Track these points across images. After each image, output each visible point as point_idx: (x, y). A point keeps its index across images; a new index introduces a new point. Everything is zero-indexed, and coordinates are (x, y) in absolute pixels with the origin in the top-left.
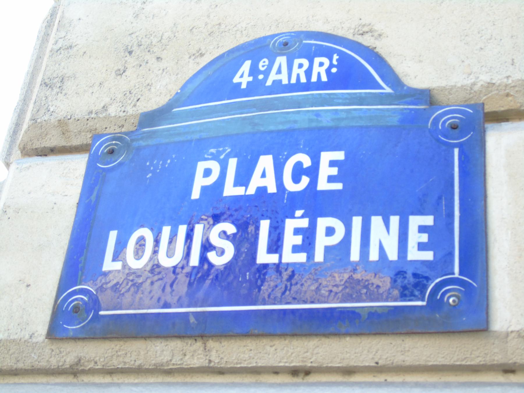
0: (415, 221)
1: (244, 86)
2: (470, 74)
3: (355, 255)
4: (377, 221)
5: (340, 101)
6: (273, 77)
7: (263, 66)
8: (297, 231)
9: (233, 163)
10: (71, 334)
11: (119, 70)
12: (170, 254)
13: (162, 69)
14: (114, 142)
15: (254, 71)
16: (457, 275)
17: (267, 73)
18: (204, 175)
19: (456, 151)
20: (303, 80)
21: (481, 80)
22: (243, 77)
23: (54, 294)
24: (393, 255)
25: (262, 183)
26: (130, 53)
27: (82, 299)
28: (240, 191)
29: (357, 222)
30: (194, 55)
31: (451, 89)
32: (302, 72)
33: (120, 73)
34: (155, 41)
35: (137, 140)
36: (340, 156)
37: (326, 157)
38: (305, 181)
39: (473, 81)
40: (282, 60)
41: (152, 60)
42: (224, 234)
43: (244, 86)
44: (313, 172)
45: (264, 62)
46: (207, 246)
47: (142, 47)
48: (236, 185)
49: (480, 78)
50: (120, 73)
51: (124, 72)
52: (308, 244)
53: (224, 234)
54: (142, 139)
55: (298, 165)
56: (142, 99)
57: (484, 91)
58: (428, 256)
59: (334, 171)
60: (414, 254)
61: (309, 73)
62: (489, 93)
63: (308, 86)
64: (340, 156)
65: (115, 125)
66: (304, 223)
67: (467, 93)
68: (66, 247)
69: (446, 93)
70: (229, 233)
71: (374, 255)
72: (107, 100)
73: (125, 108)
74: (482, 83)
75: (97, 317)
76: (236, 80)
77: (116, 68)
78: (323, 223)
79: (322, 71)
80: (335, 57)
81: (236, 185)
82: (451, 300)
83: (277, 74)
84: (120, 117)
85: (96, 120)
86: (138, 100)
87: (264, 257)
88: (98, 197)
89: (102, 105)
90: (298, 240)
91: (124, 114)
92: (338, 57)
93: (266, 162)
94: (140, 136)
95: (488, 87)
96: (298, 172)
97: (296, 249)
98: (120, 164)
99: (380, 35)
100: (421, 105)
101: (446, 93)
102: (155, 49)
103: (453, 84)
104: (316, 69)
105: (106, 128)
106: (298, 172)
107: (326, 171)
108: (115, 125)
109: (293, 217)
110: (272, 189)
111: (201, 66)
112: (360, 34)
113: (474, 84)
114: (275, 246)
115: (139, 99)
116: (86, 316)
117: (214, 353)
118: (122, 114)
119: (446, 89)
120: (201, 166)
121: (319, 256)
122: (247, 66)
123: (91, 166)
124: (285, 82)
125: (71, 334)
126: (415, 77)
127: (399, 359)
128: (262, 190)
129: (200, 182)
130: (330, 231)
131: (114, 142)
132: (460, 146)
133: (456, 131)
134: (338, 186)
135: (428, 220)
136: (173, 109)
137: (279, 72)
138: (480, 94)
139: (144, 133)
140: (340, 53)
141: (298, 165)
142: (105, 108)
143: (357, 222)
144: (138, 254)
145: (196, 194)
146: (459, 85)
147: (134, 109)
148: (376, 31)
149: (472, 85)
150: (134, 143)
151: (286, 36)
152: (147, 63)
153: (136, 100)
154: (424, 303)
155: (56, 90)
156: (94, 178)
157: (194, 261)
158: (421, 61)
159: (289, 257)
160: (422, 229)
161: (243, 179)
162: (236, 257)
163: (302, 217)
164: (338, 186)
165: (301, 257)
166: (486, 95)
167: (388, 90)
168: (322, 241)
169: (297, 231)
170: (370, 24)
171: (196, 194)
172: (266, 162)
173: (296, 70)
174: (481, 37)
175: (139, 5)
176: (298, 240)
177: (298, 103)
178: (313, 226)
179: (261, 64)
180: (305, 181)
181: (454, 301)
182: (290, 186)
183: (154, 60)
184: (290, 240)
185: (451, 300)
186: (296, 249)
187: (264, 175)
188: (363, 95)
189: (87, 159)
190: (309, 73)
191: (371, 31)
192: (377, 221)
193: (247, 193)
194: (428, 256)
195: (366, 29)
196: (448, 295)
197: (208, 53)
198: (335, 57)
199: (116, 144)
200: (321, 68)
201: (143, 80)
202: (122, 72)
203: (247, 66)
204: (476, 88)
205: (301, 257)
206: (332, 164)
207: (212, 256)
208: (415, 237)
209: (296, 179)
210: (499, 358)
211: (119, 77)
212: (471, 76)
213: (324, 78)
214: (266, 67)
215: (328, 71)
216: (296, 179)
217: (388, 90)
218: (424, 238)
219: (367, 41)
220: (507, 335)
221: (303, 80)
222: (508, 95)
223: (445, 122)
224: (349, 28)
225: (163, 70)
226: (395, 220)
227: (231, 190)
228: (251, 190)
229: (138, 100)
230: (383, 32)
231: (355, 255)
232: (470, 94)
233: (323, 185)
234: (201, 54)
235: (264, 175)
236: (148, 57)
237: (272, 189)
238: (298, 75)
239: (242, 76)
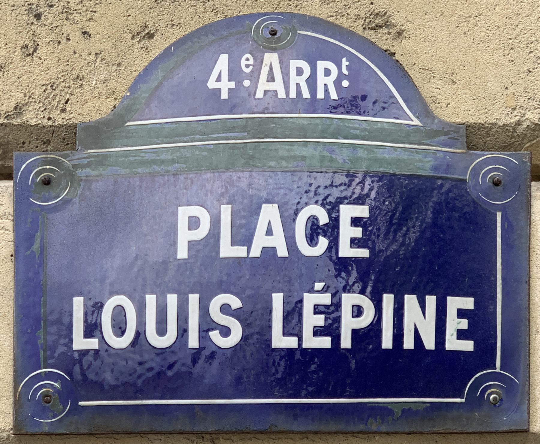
0: (455, 303)
1: (224, 95)
2: (514, 109)
3: (387, 342)
4: (410, 301)
5: (358, 132)
6: (263, 85)
7: (247, 66)
9: (226, 212)
10: (46, 429)
11: (27, 46)
12: (162, 331)
13: (93, 53)
14: (48, 167)
15: (235, 73)
16: (498, 370)
17: (255, 76)
19: (499, 215)
20: (306, 94)
21: (527, 119)
24: (430, 344)
25: (269, 242)
26: (38, 16)
27: (52, 385)
28: (240, 252)
29: (388, 300)
30: (138, 34)
31: (491, 129)
35: (83, 167)
37: (347, 212)
38: (323, 242)
39: (517, 118)
42: (225, 309)
43: (224, 95)
44: (332, 230)
45: (248, 59)
46: (207, 325)
47: (54, 9)
48: (233, 244)
49: (527, 116)
51: (35, 51)
53: (225, 309)
54: (89, 165)
55: (313, 221)
56: (73, 99)
57: (529, 135)
58: (468, 346)
60: (452, 343)
61: (312, 82)
62: (535, 139)
63: (313, 104)
65: (37, 139)
66: (326, 299)
67: (508, 136)
68: (11, 316)
69: (484, 133)
70: (234, 307)
71: (408, 343)
72: (18, 97)
73: (49, 113)
74: (528, 123)
77: (20, 43)
79: (330, 81)
80: (345, 63)
81: (233, 244)
82: (492, 397)
83: (268, 81)
84: (44, 127)
85: (8, 129)
86: (66, 103)
87: (281, 341)
88: (42, 249)
89: (13, 105)
90: (320, 320)
91: (50, 123)
92: (347, 63)
93: (270, 214)
94: (85, 162)
95: (534, 130)
96: (314, 231)
97: (318, 332)
99: (399, 34)
100: (457, 148)
101: (484, 133)
102: (77, 17)
103: (494, 121)
105: (24, 143)
107: (348, 232)
108: (37, 139)
109: (311, 290)
110: (282, 252)
112: (372, 29)
113: (519, 123)
115: (68, 100)
116: (61, 407)
118: (45, 122)
119: (484, 128)
120: (184, 213)
121: (346, 343)
125: (47, 428)
126: (447, 106)
128: (269, 252)
129: (185, 237)
131: (48, 167)
132: (503, 209)
133: (500, 188)
134: (364, 253)
135: (468, 303)
136: (126, 123)
137: (271, 78)
138: (523, 140)
139: (90, 156)
140: (351, 57)
141: (313, 221)
142: (18, 109)
143: (388, 300)
145: (182, 253)
146: (501, 123)
147: (63, 115)
148: (394, 25)
149: (516, 124)
150: (79, 171)
151: (272, 19)
152: (68, 40)
153: (63, 101)
154: (463, 400)
156: (29, 220)
157: (193, 342)
158: (454, 82)
159: (311, 342)
160: (461, 313)
162: (245, 338)
163: (324, 290)
164: (364, 253)
165: (325, 342)
166: (529, 141)
167: (416, 122)
170: (385, 13)
171: (182, 253)
172: (270, 214)
174: (530, 52)
176: (320, 320)
177: (303, 131)
179: (243, 62)
180: (323, 242)
181: (495, 398)
183: (78, 34)
184: (311, 320)
185: (492, 397)
186: (318, 332)
187: (269, 232)
188: (386, 126)
189: (11, 190)
190: (312, 82)
192: (410, 301)
193: (251, 255)
194: (468, 346)
195: (379, 21)
196: (489, 391)
197: (159, 33)
198: (345, 63)
199: (51, 170)
200: (329, 78)
201: (69, 68)
202: (32, 50)
204: (520, 129)
207: (215, 336)
208: (454, 324)
209: (312, 240)
211: (28, 59)
212: (515, 113)
213: (334, 95)
214: (251, 67)
215: (337, 83)
216: (312, 240)
217: (416, 122)
218: (464, 324)
219: (382, 40)
224: (358, 17)
225: (97, 54)
226: (431, 301)
227: (228, 250)
228: (255, 252)
229: (66, 103)
230: (403, 28)
231: (387, 342)
232: (511, 138)
233: (346, 250)
234: (148, 33)
235: (269, 232)
236: (67, 29)
237: (282, 252)
238: (298, 85)
239: (219, 79)
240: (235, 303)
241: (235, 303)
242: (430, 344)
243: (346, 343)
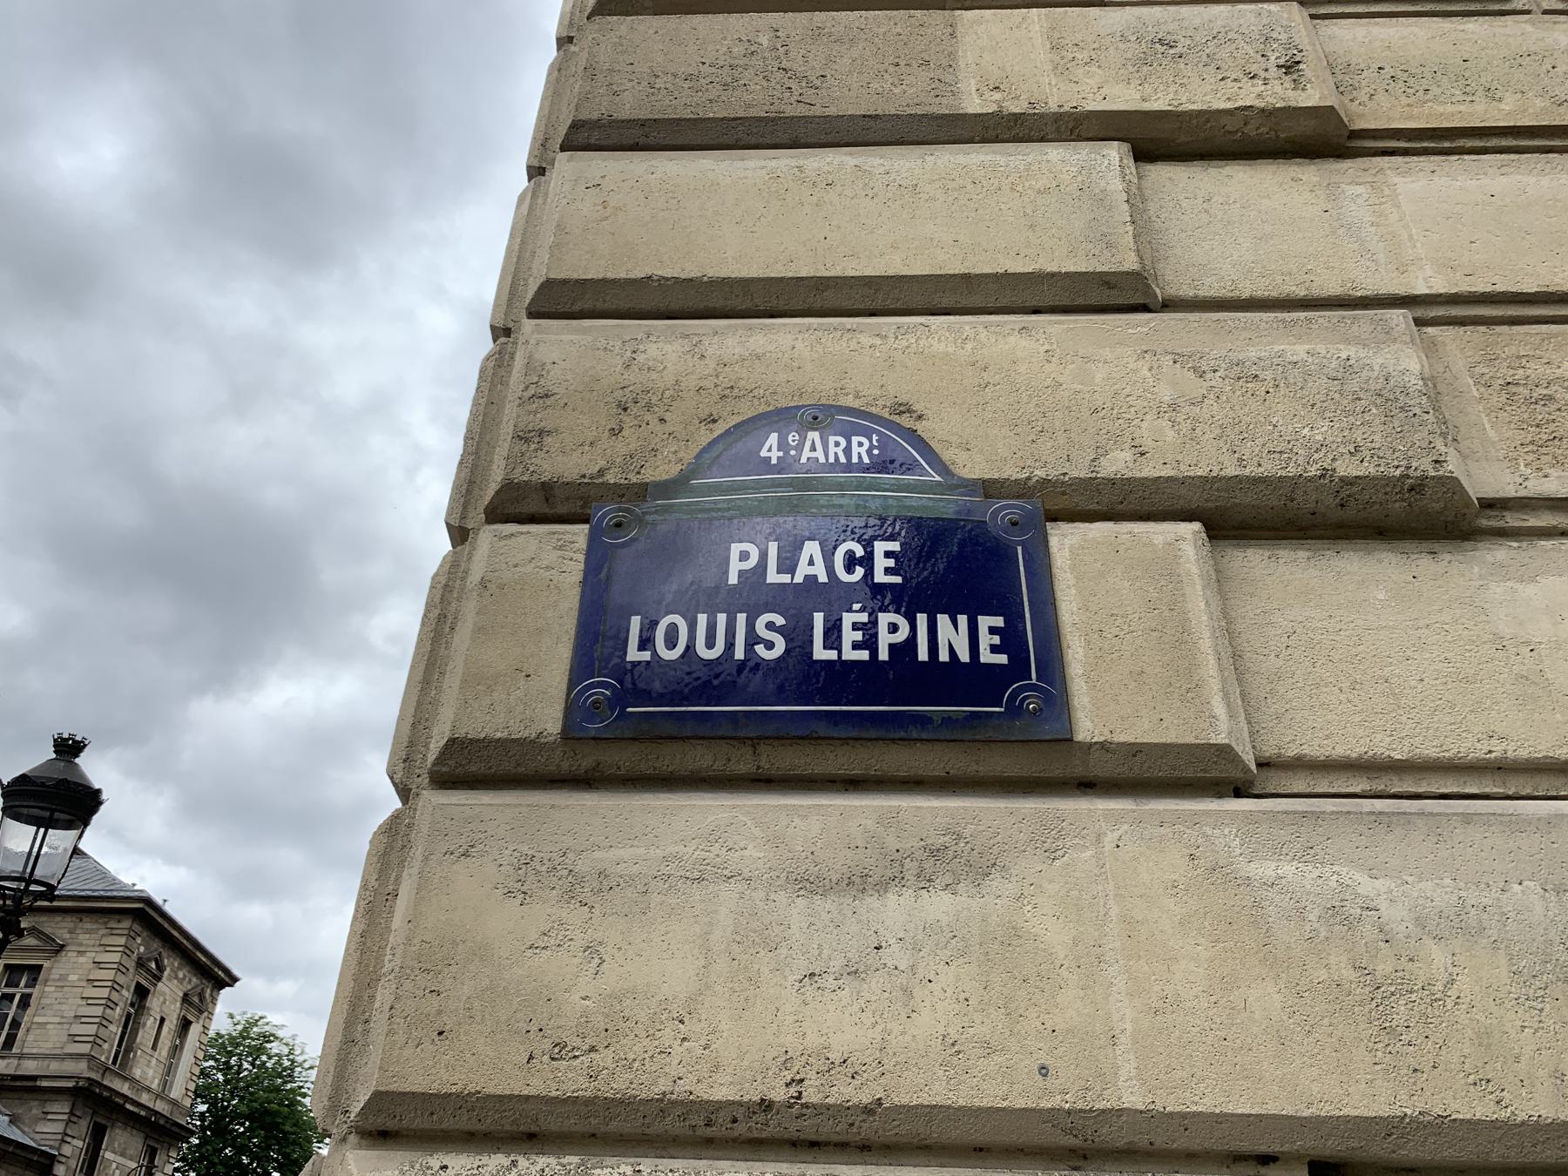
0: (985, 622)
1: (774, 461)
3: (923, 655)
4: (943, 620)
6: (806, 454)
8: (856, 627)
9: (773, 548)
10: (593, 734)
12: (710, 644)
15: (783, 445)
17: (800, 448)
18: (740, 558)
19: (1019, 549)
20: (843, 460)
22: (770, 448)
23: (564, 686)
24: (964, 657)
26: (625, 409)
28: (786, 578)
32: (840, 450)
33: (615, 433)
34: (654, 399)
36: (895, 546)
38: (860, 572)
40: (814, 436)
41: (654, 421)
42: (770, 626)
43: (774, 461)
44: (868, 561)
46: (752, 639)
50: (615, 433)
52: (870, 643)
53: (770, 626)
55: (850, 556)
59: (891, 563)
61: (848, 451)
63: (849, 467)
64: (895, 546)
66: (864, 618)
72: (602, 463)
75: (623, 714)
76: (764, 453)
78: (884, 619)
87: (820, 653)
93: (812, 548)
96: (851, 562)
98: (633, 540)
104: (855, 449)
106: (851, 562)
107: (881, 563)
109: (850, 610)
110: (823, 578)
111: (716, 434)
113: (1029, 478)
114: (646, 643)
117: (764, 758)
120: (736, 548)
121: (883, 655)
122: (773, 438)
123: (593, 539)
124: (822, 460)
127: (645, 768)
129: (735, 567)
130: (894, 628)
132: (1023, 543)
134: (898, 580)
135: (999, 622)
137: (813, 449)
140: (879, 433)
141: (850, 556)
142: (601, 472)
143: (922, 619)
144: (671, 643)
145: (733, 579)
155: (533, 447)
157: (739, 654)
159: (850, 654)
160: (992, 631)
161: (788, 566)
162: (787, 651)
163: (862, 610)
164: (898, 580)
165: (864, 655)
168: (885, 640)
169: (856, 627)
171: (733, 579)
172: (812, 548)
173: (832, 449)
175: (629, 354)
177: (841, 486)
178: (874, 623)
179: (790, 438)
180: (860, 572)
182: (844, 577)
184: (849, 636)
187: (811, 563)
190: (848, 451)
191: (909, 411)
192: (943, 620)
194: (1002, 659)
198: (875, 437)
200: (861, 449)
203: (773, 438)
204: (1030, 483)
205: (864, 655)
206: (888, 554)
207: (760, 649)
208: (985, 640)
209: (849, 568)
210: (1079, 771)
213: (866, 460)
215: (869, 452)
216: (849, 568)
220: (1091, 745)
221: (843, 460)
222: (1064, 493)
223: (1003, 518)
227: (773, 577)
228: (799, 579)
231: (923, 655)
233: (880, 577)
235: (811, 563)
236: (648, 417)
240: (779, 620)
241: (779, 620)
242: (964, 657)
243: (883, 655)
